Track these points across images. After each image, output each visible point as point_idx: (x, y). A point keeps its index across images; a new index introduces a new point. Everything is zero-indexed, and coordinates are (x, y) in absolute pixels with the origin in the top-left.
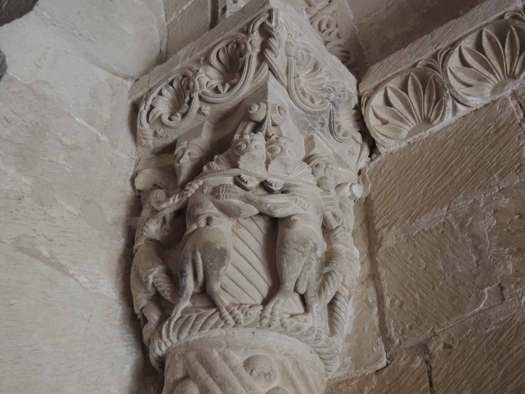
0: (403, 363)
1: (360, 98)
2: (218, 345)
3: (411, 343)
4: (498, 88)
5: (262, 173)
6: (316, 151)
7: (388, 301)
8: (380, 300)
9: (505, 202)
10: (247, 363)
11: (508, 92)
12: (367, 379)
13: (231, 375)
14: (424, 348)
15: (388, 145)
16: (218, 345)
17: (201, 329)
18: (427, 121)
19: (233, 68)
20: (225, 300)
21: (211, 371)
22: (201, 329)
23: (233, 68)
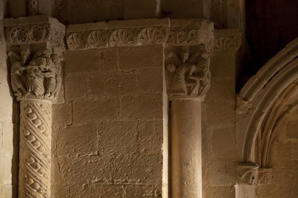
0: (68, 103)
1: (66, 34)
2: (35, 102)
3: (70, 100)
4: (98, 46)
5: (45, 67)
6: (54, 53)
7: (66, 90)
8: (64, 89)
9: (92, 77)
10: (41, 105)
11: (100, 48)
12: (60, 105)
13: (37, 107)
14: (72, 102)
15: (71, 48)
16: (35, 102)
17: (48, 168)
18: (81, 47)
19: (37, 36)
20: (37, 94)
21: (34, 107)
22: (48, 168)
23: (37, 36)
